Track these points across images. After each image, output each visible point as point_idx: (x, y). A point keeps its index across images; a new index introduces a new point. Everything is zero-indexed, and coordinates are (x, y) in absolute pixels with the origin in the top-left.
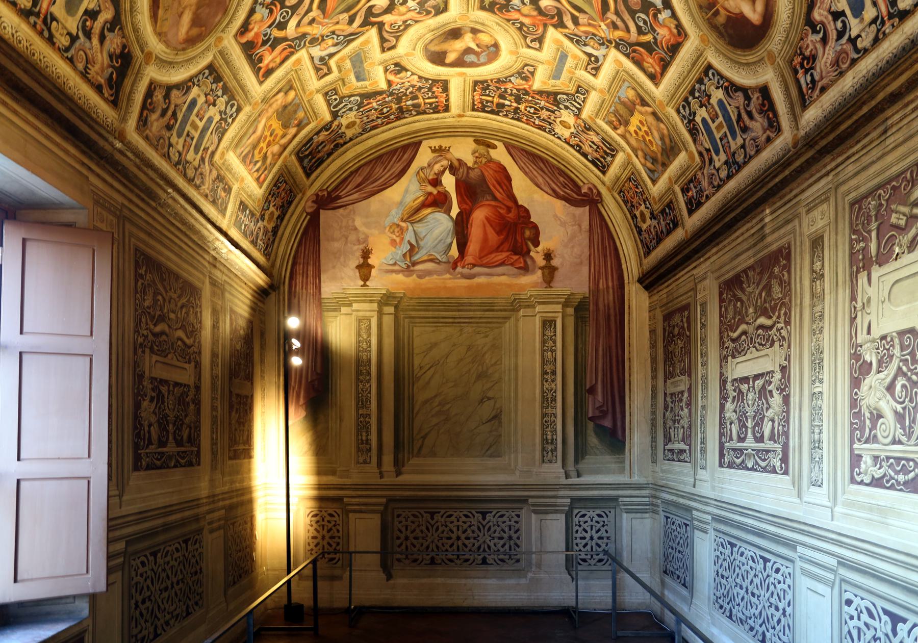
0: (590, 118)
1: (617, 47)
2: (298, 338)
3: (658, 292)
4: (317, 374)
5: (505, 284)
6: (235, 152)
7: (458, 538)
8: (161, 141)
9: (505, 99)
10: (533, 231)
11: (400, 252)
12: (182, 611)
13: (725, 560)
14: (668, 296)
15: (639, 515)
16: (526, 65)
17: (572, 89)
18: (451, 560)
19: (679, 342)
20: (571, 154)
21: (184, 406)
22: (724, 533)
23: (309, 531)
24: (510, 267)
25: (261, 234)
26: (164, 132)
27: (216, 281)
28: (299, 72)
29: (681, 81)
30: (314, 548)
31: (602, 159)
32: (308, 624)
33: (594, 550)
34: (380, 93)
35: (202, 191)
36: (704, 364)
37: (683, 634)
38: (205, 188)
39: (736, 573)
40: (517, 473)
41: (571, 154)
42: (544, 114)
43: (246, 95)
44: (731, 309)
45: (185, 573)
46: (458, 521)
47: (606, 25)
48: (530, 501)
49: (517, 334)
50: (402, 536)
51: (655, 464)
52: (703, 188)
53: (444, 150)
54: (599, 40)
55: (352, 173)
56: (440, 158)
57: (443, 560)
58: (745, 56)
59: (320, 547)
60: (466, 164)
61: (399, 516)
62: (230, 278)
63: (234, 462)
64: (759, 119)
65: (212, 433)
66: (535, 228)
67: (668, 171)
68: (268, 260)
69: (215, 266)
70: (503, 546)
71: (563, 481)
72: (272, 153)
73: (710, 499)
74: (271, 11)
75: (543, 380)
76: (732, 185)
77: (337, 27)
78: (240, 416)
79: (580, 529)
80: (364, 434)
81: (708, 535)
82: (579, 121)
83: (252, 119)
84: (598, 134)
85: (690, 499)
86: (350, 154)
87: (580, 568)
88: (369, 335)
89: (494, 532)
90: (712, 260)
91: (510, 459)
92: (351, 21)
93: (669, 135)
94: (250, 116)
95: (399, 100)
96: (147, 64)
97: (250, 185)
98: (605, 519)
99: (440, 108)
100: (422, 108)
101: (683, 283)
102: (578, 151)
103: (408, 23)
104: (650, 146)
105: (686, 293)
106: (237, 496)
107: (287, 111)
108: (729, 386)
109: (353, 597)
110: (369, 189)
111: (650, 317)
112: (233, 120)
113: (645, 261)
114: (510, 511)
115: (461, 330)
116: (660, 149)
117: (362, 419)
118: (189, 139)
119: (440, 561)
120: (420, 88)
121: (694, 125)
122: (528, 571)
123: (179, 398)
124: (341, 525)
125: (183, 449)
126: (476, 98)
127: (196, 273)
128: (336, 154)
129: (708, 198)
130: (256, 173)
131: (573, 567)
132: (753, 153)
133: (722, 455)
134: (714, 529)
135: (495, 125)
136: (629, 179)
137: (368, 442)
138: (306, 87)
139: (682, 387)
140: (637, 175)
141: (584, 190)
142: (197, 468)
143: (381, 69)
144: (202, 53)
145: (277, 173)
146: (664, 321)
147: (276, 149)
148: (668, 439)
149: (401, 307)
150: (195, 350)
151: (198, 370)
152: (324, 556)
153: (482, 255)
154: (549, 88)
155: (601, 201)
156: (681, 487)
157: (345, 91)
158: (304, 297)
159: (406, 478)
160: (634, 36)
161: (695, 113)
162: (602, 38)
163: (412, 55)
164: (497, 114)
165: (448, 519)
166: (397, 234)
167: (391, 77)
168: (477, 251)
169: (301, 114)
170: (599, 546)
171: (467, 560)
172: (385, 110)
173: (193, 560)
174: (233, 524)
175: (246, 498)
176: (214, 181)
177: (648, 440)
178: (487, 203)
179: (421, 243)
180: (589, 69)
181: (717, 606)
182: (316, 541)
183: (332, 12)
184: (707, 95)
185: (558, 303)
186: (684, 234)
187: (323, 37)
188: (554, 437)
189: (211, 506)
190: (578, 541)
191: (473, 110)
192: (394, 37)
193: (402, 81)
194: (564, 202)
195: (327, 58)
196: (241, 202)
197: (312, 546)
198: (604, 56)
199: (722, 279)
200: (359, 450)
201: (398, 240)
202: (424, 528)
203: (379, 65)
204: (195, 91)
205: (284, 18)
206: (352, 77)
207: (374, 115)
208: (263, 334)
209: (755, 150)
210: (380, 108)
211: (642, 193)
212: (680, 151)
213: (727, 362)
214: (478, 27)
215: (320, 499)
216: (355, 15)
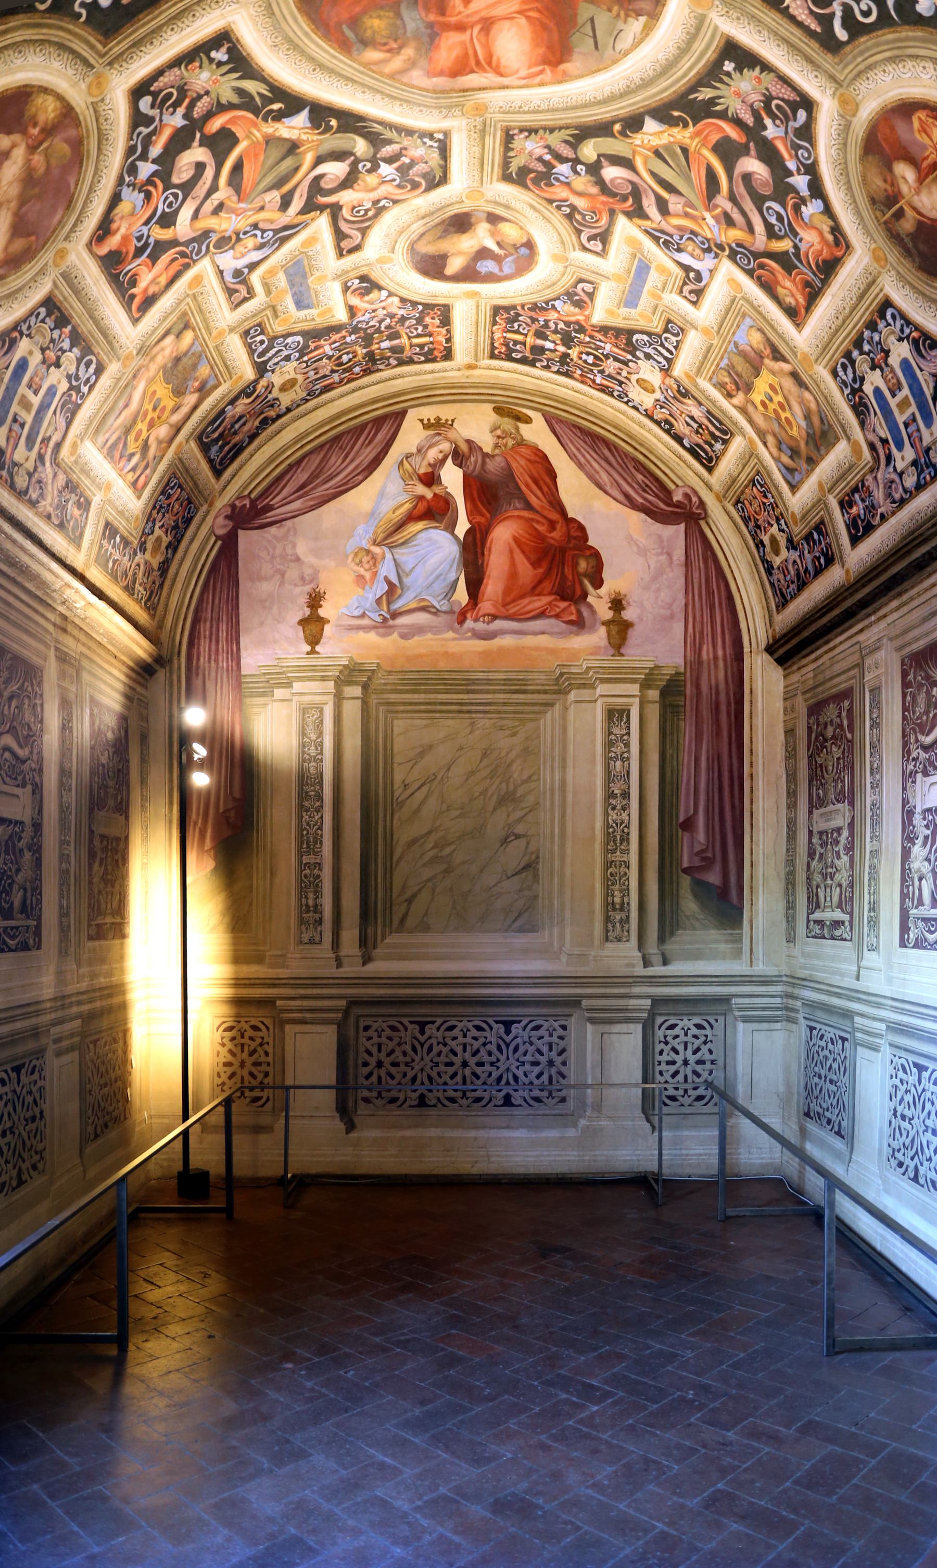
1: (733, 256)
2: (202, 742)
3: (799, 669)
4: (234, 799)
5: (546, 649)
6: (94, 441)
7: (465, 1064)
9: (546, 338)
10: (593, 562)
12: (11, 1178)
13: (907, 1091)
14: (815, 676)
15: (765, 1026)
16: (581, 281)
18: (452, 1100)
19: (834, 749)
21: (14, 854)
22: (906, 1050)
23: (218, 1053)
25: (140, 575)
27: (66, 654)
28: (199, 299)
29: (839, 322)
30: (227, 1081)
31: (706, 447)
32: (217, 1201)
33: (690, 1080)
35: (40, 510)
36: (876, 786)
37: (838, 1211)
38: (47, 504)
39: (926, 1111)
40: (564, 959)
42: (611, 366)
43: (110, 343)
44: (922, 698)
45: (16, 1118)
46: (465, 1036)
47: (715, 218)
48: (585, 1003)
49: (564, 729)
50: (373, 1061)
51: (791, 945)
52: (875, 502)
53: (443, 425)
54: (703, 243)
55: (290, 467)
56: (437, 438)
57: (439, 1100)
59: (237, 1078)
60: (481, 449)
61: (366, 1028)
62: (89, 648)
63: (97, 943)
65: (61, 896)
66: (596, 556)
67: (818, 471)
68: (153, 616)
69: (65, 630)
70: (538, 1077)
71: (640, 971)
72: (157, 439)
73: (885, 997)
74: (148, 196)
75: (608, 806)
78: (106, 869)
79: (667, 1049)
80: (311, 895)
81: (880, 1054)
83: (122, 383)
84: (700, 404)
85: (850, 999)
86: (287, 436)
87: (665, 1110)
88: (321, 734)
89: (525, 1054)
90: (889, 619)
91: (551, 935)
92: (285, 203)
93: (819, 412)
94: (119, 380)
95: (368, 340)
98: (708, 1032)
99: (436, 353)
100: (407, 353)
101: (842, 656)
102: (668, 432)
103: (381, 204)
104: (787, 428)
106: (101, 998)
107: (180, 367)
108: (918, 820)
109: (290, 1159)
111: (785, 709)
112: (91, 388)
114: (551, 1019)
116: (804, 434)
117: (307, 872)
118: (16, 427)
119: (433, 1102)
120: (403, 319)
121: (861, 398)
122: (580, 1117)
123: (7, 842)
124: (271, 1043)
125: (12, 923)
126: (497, 335)
129: (883, 518)
130: (131, 474)
131: (653, 1109)
133: (904, 928)
134: (890, 1045)
136: (753, 482)
137: (317, 909)
138: (212, 324)
139: (838, 822)
141: (678, 497)
142: (35, 952)
143: (337, 287)
144: (34, 279)
145: (165, 472)
146: (809, 716)
147: (163, 431)
148: (814, 904)
149: (372, 687)
150: (33, 765)
151: (38, 797)
152: (243, 1093)
153: (508, 600)
154: (618, 322)
155: (706, 517)
156: (836, 980)
157: (277, 327)
158: (213, 674)
159: (379, 967)
160: (760, 241)
161: (862, 379)
162: (708, 240)
163: (389, 260)
164: (532, 364)
165: (448, 1034)
166: (367, 566)
167: (355, 301)
168: (500, 593)
169: (204, 371)
170: (698, 1075)
171: (478, 1100)
172: (345, 358)
173: (29, 1099)
174: (95, 1042)
175: (116, 1000)
176: (60, 492)
177: (781, 906)
178: (516, 513)
179: (406, 581)
180: (686, 293)
181: (894, 1163)
182: (229, 1070)
183: (252, 189)
184: (883, 350)
186: (844, 576)
188: (626, 900)
189: (60, 1014)
190: (664, 1067)
191: (492, 356)
192: (358, 229)
193: (374, 307)
194: (643, 516)
195: (246, 271)
196: (107, 524)
197: (224, 1077)
198: (711, 271)
199: (907, 650)
200: (301, 921)
201: (368, 575)
202: (408, 1048)
203: (334, 279)
204: (24, 345)
206: (289, 303)
207: (326, 366)
208: (144, 738)
210: (337, 354)
211: (774, 506)
212: (837, 439)
213: (914, 782)
215: (238, 1002)
216: (291, 193)
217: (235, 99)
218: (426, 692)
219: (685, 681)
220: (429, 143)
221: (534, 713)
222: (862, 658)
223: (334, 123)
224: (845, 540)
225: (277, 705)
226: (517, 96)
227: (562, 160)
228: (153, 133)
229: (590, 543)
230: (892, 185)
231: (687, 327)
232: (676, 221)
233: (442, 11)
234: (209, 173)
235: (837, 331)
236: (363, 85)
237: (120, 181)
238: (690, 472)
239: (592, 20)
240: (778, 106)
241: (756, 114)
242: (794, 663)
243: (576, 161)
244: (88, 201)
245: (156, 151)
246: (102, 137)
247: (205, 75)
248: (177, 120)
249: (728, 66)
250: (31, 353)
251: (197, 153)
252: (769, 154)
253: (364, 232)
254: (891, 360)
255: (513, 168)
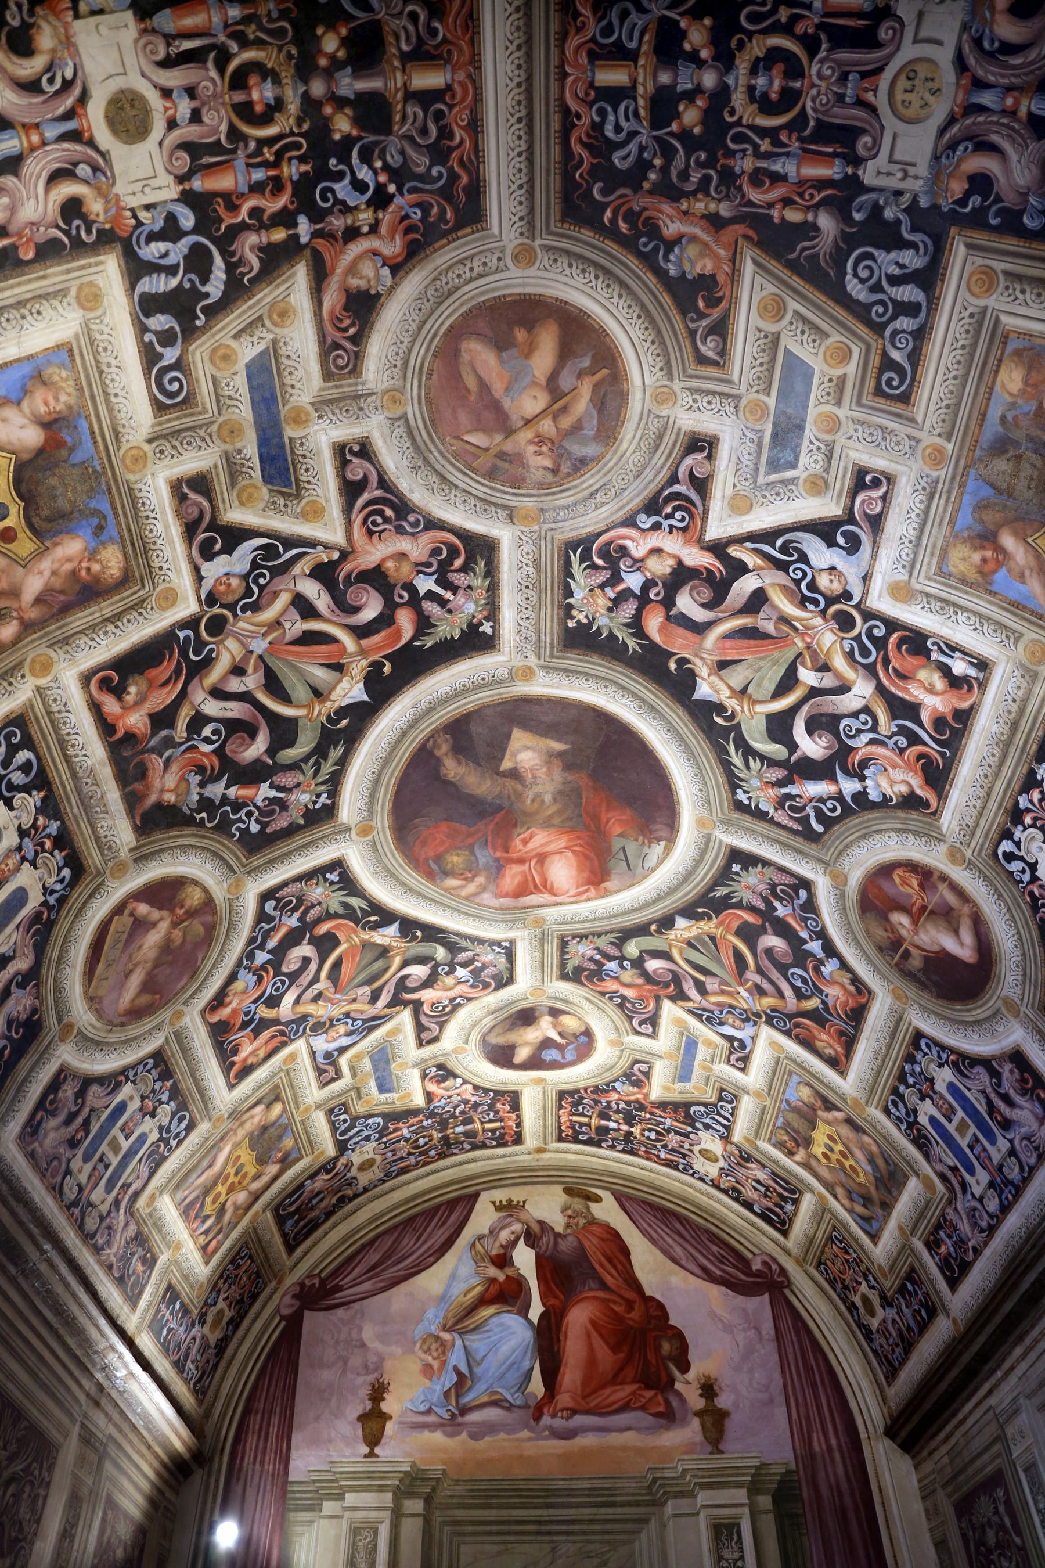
0: (747, 1140)
1: (769, 1022)
3: (930, 1454)
8: (55, 1163)
9: (609, 1119)
11: (438, 1388)
14: (952, 1461)
16: (637, 1062)
17: (711, 1096)
20: (725, 1206)
24: (639, 1414)
25: (194, 1351)
26: (65, 1152)
31: (777, 1210)
34: (415, 1112)
38: (111, 1253)
41: (725, 1206)
42: (673, 1140)
43: (206, 1107)
49: (664, 1555)
53: (515, 1207)
55: (363, 1246)
56: (509, 1220)
58: (969, 1011)
60: (552, 1229)
62: (121, 1431)
64: (1024, 1104)
66: (678, 1336)
68: (200, 1402)
69: (97, 1404)
72: (234, 1204)
74: (260, 979)
76: (1013, 1222)
77: (354, 1006)
82: (729, 1147)
83: (210, 1143)
84: (764, 1166)
86: (363, 1216)
92: (375, 998)
94: (207, 1139)
95: (443, 1125)
96: (62, 1040)
97: (190, 1256)
99: (507, 1138)
100: (480, 1138)
102: (736, 1200)
103: (458, 1000)
105: (986, 1449)
107: (266, 1136)
110: (390, 1273)
113: (891, 1392)
115: (553, 1550)
116: (872, 1179)
118: (101, 1167)
120: (476, 1105)
121: (918, 1130)
126: (564, 1119)
127: (57, 1411)
128: (339, 1214)
129: (977, 1252)
130: (203, 1237)
132: (1033, 1161)
135: (596, 1163)
136: (830, 1239)
140: (843, 1231)
141: (757, 1266)
143: (416, 1074)
144: (149, 1032)
145: (238, 1240)
147: (241, 1197)
154: (675, 1097)
155: (789, 1284)
160: (791, 1003)
161: (915, 1111)
163: (464, 1050)
164: (598, 1144)
166: (435, 1354)
167: (432, 1087)
168: (579, 1383)
169: (288, 1143)
172: (422, 1141)
176: (128, 1243)
178: (592, 1294)
179: (477, 1370)
183: (349, 983)
184: (927, 1079)
185: (738, 1485)
186: (952, 1326)
187: (331, 1020)
191: (560, 1139)
193: (449, 1093)
194: (723, 1288)
196: (170, 1287)
201: (436, 1364)
204: (127, 1089)
205: (277, 990)
207: (404, 1148)
209: (1035, 1155)
210: (414, 1137)
211: (858, 1261)
214: (560, 1006)
216: (381, 989)
217: (341, 910)
218: (500, 1507)
219: (799, 1481)
220: (498, 950)
221: (624, 1532)
222: (1001, 1427)
223: (419, 934)
224: (942, 1285)
225: (325, 1522)
226: (568, 910)
227: (610, 958)
228: (272, 929)
229: (672, 1322)
230: (893, 932)
231: (740, 1093)
232: (714, 999)
233: (507, 850)
234: (313, 967)
235: (879, 1071)
236: (444, 905)
237: (239, 963)
238: (765, 1239)
239: (623, 848)
240: (782, 891)
241: (765, 900)
242: (922, 1448)
243: (622, 958)
244: (210, 974)
245: (272, 944)
246: (231, 926)
247: (320, 890)
248: (293, 922)
249: (736, 868)
250: (131, 1098)
251: (306, 950)
252: (783, 929)
253: (442, 1025)
254: (937, 1087)
255: (569, 968)
